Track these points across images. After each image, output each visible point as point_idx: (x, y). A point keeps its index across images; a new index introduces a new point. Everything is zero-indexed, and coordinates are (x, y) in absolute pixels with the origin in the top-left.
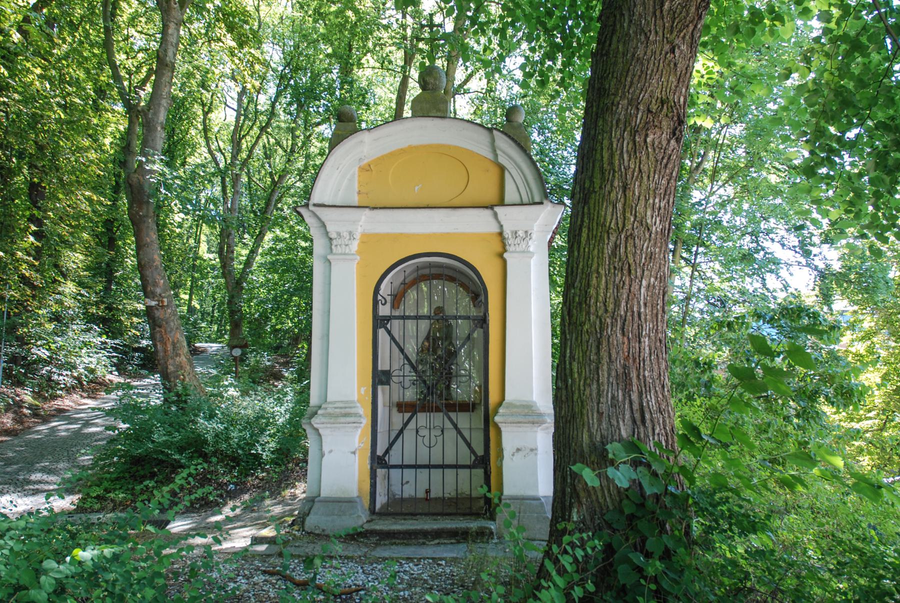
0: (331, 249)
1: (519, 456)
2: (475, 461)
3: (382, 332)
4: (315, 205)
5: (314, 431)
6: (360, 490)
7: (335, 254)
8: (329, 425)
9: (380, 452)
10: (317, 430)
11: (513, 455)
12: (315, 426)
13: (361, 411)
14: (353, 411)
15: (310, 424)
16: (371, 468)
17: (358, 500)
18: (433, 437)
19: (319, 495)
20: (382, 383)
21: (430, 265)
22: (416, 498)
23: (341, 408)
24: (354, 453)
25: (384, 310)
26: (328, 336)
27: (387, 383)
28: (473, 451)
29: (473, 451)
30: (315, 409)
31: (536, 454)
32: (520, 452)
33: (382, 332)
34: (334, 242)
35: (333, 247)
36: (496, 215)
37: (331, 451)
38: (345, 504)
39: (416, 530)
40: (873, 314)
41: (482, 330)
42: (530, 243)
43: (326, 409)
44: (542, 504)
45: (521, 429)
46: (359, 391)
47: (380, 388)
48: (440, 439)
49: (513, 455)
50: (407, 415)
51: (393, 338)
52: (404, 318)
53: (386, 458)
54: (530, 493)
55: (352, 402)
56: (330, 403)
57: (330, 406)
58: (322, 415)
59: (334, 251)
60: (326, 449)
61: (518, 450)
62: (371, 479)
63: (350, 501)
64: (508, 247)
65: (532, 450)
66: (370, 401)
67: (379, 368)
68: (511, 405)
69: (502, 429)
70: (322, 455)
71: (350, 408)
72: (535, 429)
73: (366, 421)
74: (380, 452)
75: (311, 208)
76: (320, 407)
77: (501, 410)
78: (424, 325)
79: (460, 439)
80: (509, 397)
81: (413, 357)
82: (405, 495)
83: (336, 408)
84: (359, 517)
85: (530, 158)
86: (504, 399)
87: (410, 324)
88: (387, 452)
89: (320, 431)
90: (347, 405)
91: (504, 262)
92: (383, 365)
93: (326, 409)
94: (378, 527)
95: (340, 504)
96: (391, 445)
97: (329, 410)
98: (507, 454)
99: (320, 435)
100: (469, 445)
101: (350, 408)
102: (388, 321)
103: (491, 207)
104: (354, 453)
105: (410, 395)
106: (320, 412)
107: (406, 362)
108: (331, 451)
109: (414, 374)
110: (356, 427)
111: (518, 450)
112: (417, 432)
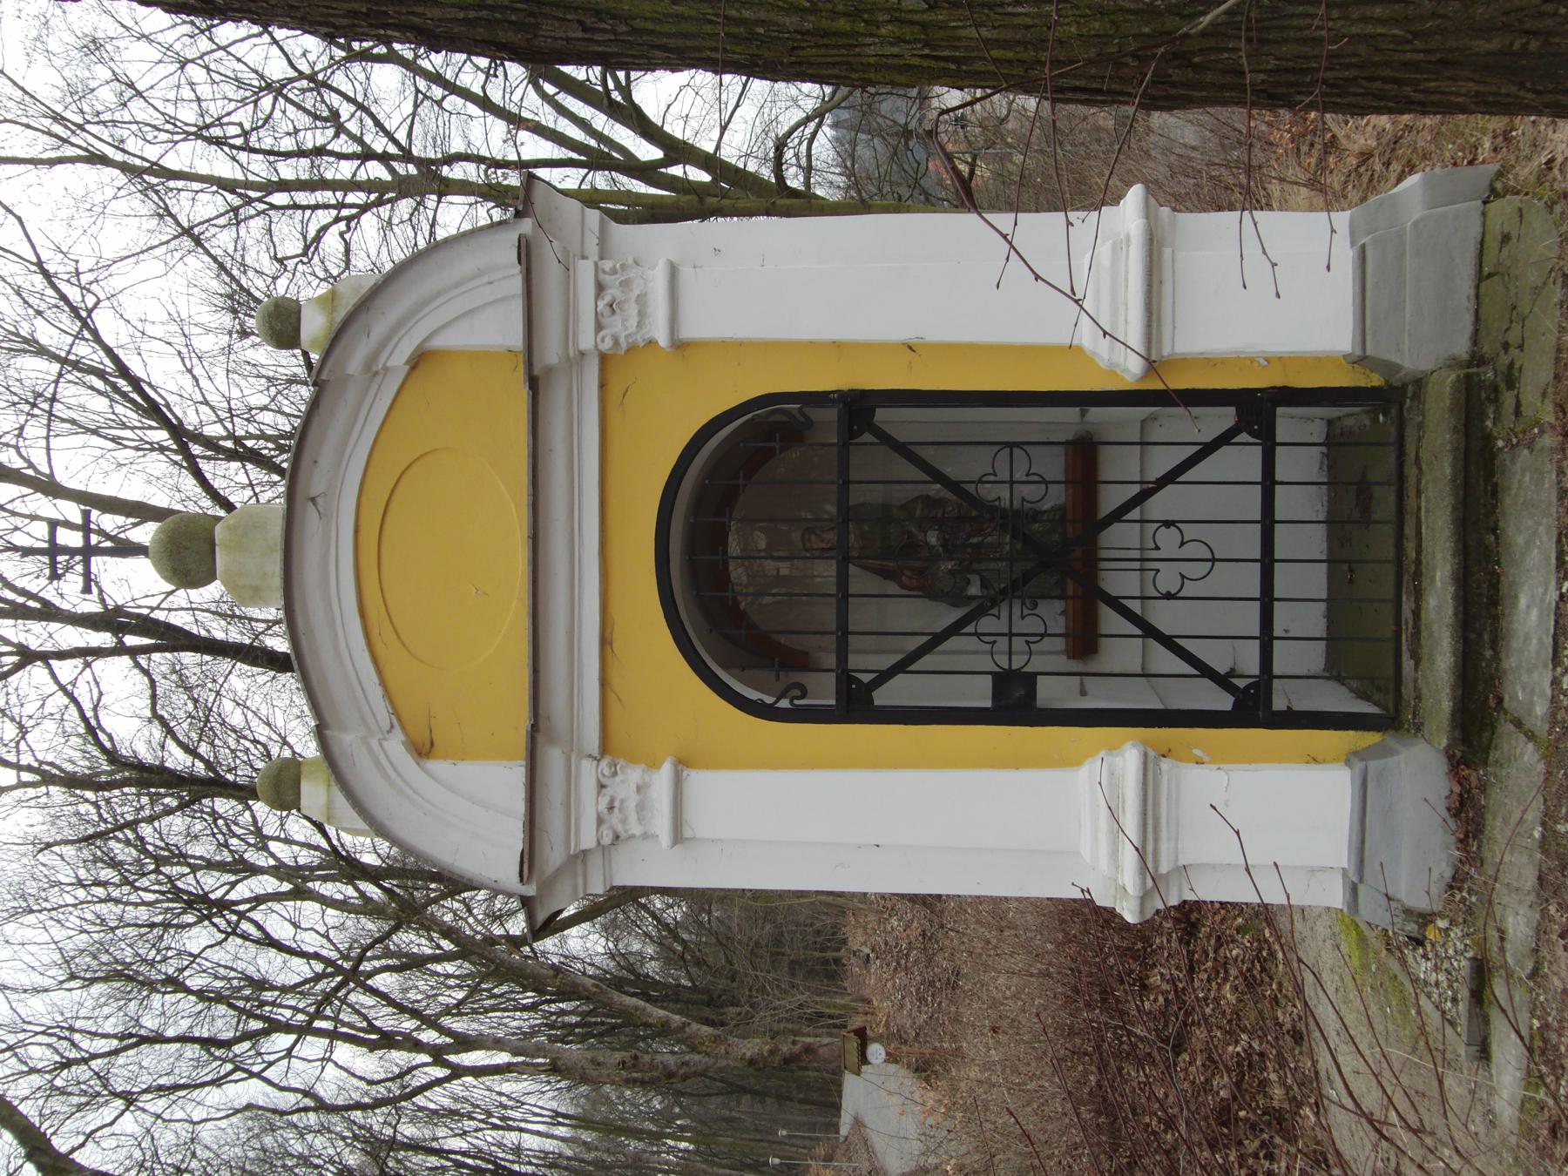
2: (1252, 433)
3: (882, 697)
18: (1187, 552)
21: (692, 532)
22: (1330, 600)
25: (824, 692)
27: (1029, 680)
28: (1225, 439)
29: (1225, 439)
33: (882, 697)
40: (612, 956)
47: (1279, 704)
48: (1190, 531)
50: (1110, 621)
51: (900, 667)
52: (843, 633)
67: (988, 703)
74: (1225, 702)
78: (860, 581)
81: (949, 615)
82: (1318, 627)
87: (862, 615)
92: (979, 694)
96: (1205, 671)
100: (1207, 449)
105: (1053, 615)
107: (970, 629)
109: (1004, 607)
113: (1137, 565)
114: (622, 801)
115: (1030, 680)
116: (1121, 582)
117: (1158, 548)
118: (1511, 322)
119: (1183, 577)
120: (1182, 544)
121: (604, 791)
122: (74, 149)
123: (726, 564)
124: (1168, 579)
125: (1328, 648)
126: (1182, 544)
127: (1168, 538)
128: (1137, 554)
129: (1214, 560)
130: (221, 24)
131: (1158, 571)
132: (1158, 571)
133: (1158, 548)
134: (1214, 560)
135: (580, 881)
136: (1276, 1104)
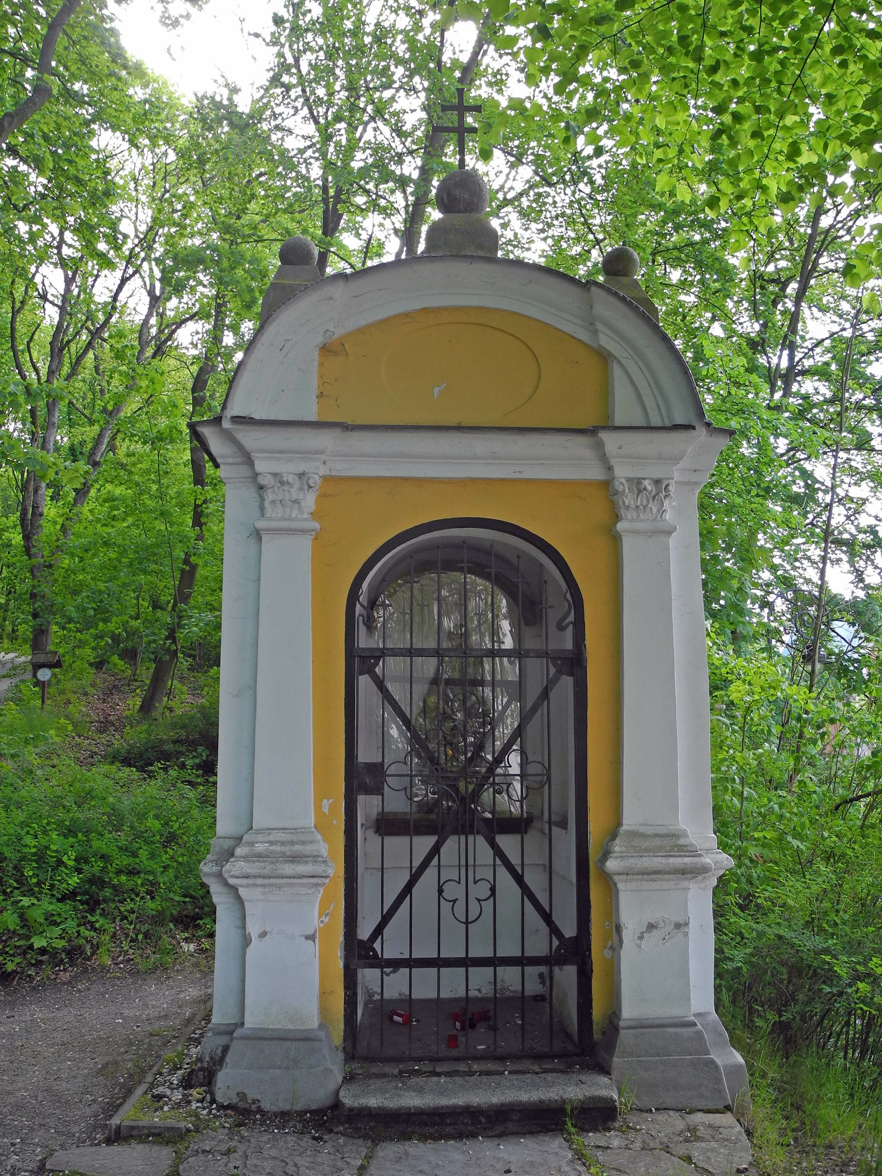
0: (262, 509)
1: (652, 940)
4: (238, 420)
5: (224, 890)
6: (324, 1011)
7: (271, 519)
8: (259, 881)
9: (364, 932)
10: (234, 889)
11: (641, 938)
12: (231, 881)
13: (323, 849)
14: (308, 849)
15: (220, 875)
16: (346, 967)
17: (322, 1034)
18: (473, 904)
19: (243, 1024)
20: (368, 791)
23: (283, 843)
24: (311, 938)
26: (253, 688)
28: (554, 930)
29: (554, 930)
30: (227, 844)
31: (686, 934)
32: (655, 932)
33: (364, 682)
34: (269, 496)
35: (267, 504)
36: (600, 446)
37: (263, 935)
38: (298, 1044)
39: (455, 1107)
41: (570, 680)
42: (666, 503)
43: (252, 844)
44: (699, 1034)
45: (655, 885)
46: (318, 806)
47: (361, 799)
48: (488, 906)
49: (641, 938)
53: (377, 946)
54: (675, 1012)
55: (304, 830)
56: (258, 832)
57: (260, 838)
58: (245, 858)
59: (268, 513)
60: (253, 929)
61: (651, 927)
62: (346, 988)
63: (305, 1038)
64: (623, 512)
65: (678, 926)
66: (343, 828)
68: (634, 834)
69: (621, 886)
70: (246, 941)
71: (303, 843)
72: (685, 884)
73: (337, 869)
74: (364, 932)
75: (226, 424)
76: (239, 839)
77: (618, 847)
79: (528, 905)
80: (630, 821)
83: (272, 843)
84: (327, 1071)
85: (656, 328)
86: (619, 824)
88: (378, 931)
89: (242, 892)
90: (294, 838)
91: (616, 540)
92: (366, 755)
93: (252, 844)
94: (373, 1102)
95: (287, 1044)
97: (260, 847)
98: (628, 936)
99: (240, 901)
101: (303, 843)
102: (378, 658)
103: (592, 431)
104: (311, 938)
106: (239, 851)
108: (263, 935)
110: (316, 885)
111: (651, 927)
112: (440, 891)
113: (463, 862)
114: (268, 70)
115: (378, 790)
116: (451, 846)
117: (475, 882)
118: (689, 1159)
119: (455, 901)
120: (479, 900)
121: (297, 478)
122: (490, 694)
123: (461, 570)
124: (453, 891)
125: (431, 1000)
126: (479, 900)
127: (483, 890)
128: (471, 862)
129: (467, 923)
130: (394, 972)
131: (459, 883)
132: (459, 883)
133: (475, 882)
134: (467, 923)
135: (231, 460)
136: (206, 1065)
